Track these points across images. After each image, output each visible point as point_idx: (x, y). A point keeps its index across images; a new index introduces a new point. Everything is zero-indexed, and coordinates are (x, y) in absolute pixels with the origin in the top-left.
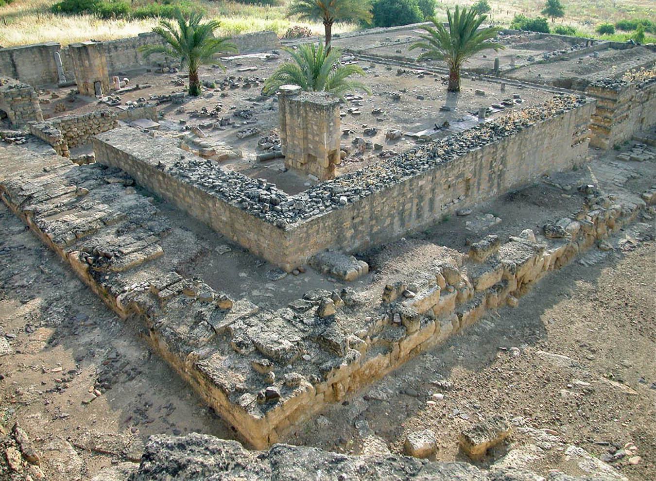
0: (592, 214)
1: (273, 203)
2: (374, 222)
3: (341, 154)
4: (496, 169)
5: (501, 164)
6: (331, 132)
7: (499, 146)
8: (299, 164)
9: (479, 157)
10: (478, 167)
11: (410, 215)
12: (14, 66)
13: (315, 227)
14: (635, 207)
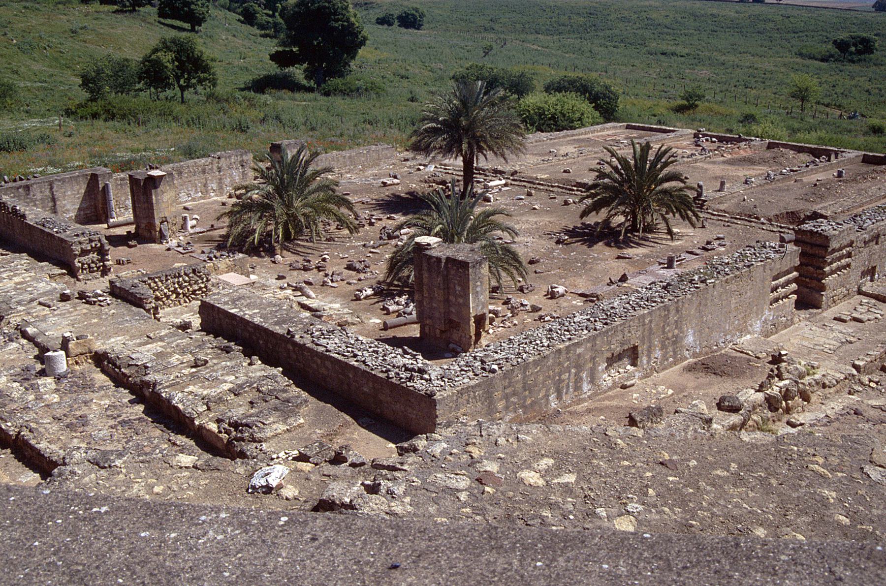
0: (781, 384)
1: (421, 371)
2: (527, 393)
3: (490, 318)
4: (670, 335)
5: (676, 328)
6: (477, 292)
7: (672, 308)
8: (438, 332)
9: (647, 321)
10: (646, 333)
11: (568, 386)
12: (54, 200)
13: (465, 397)
14: (842, 377)
